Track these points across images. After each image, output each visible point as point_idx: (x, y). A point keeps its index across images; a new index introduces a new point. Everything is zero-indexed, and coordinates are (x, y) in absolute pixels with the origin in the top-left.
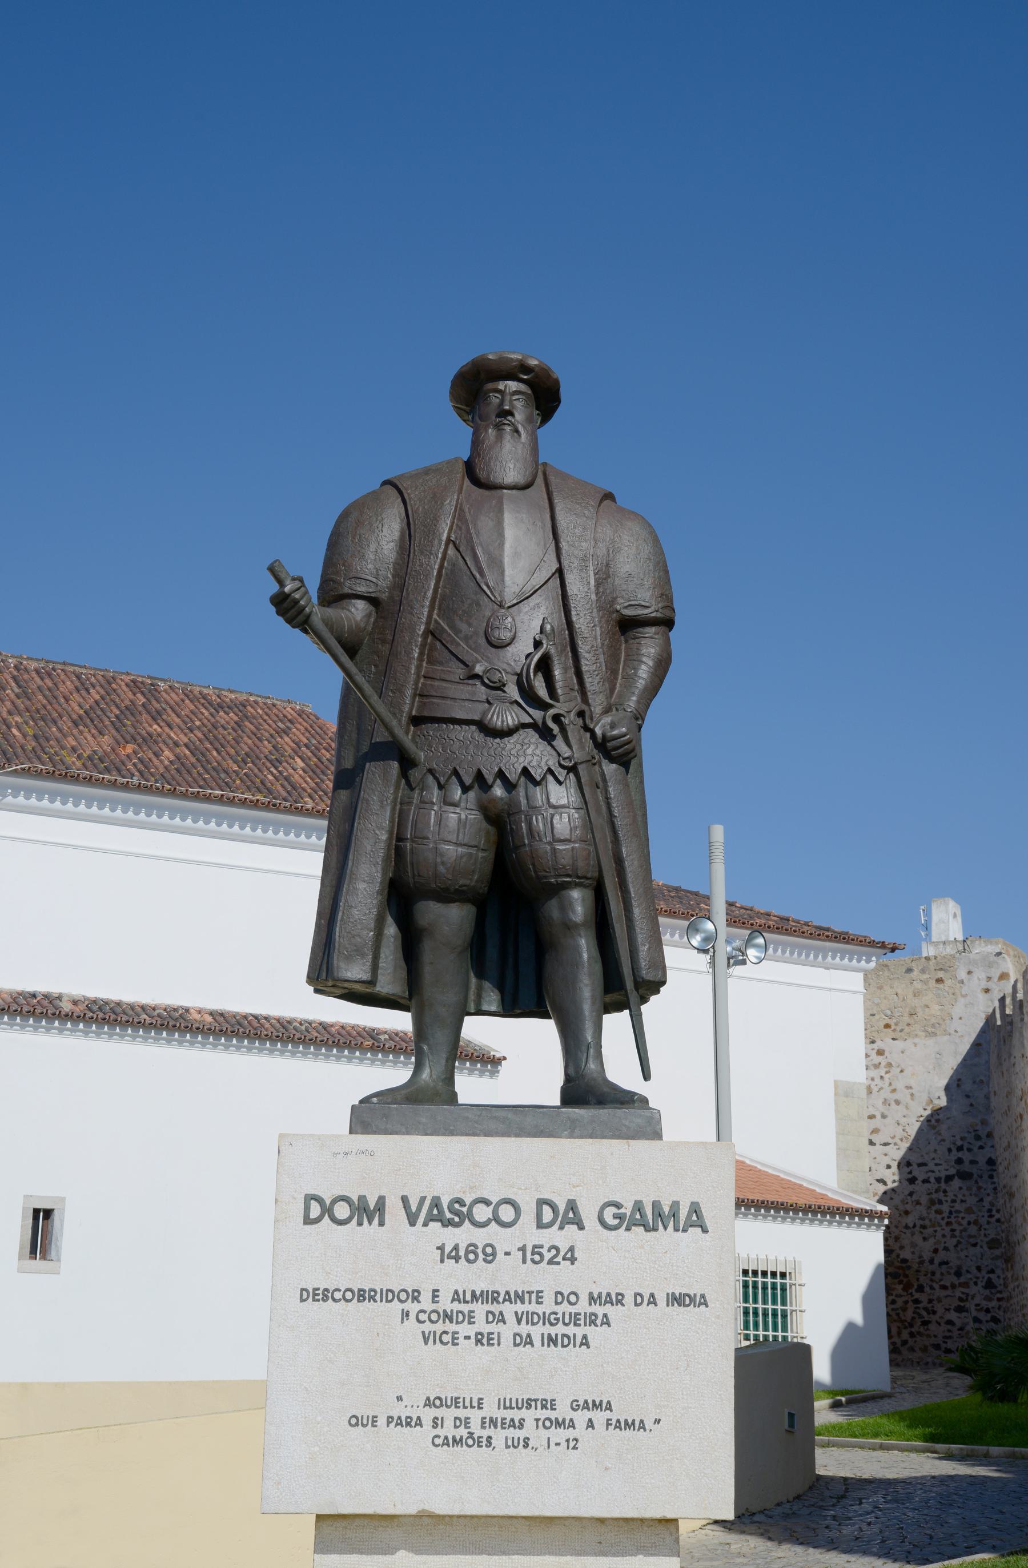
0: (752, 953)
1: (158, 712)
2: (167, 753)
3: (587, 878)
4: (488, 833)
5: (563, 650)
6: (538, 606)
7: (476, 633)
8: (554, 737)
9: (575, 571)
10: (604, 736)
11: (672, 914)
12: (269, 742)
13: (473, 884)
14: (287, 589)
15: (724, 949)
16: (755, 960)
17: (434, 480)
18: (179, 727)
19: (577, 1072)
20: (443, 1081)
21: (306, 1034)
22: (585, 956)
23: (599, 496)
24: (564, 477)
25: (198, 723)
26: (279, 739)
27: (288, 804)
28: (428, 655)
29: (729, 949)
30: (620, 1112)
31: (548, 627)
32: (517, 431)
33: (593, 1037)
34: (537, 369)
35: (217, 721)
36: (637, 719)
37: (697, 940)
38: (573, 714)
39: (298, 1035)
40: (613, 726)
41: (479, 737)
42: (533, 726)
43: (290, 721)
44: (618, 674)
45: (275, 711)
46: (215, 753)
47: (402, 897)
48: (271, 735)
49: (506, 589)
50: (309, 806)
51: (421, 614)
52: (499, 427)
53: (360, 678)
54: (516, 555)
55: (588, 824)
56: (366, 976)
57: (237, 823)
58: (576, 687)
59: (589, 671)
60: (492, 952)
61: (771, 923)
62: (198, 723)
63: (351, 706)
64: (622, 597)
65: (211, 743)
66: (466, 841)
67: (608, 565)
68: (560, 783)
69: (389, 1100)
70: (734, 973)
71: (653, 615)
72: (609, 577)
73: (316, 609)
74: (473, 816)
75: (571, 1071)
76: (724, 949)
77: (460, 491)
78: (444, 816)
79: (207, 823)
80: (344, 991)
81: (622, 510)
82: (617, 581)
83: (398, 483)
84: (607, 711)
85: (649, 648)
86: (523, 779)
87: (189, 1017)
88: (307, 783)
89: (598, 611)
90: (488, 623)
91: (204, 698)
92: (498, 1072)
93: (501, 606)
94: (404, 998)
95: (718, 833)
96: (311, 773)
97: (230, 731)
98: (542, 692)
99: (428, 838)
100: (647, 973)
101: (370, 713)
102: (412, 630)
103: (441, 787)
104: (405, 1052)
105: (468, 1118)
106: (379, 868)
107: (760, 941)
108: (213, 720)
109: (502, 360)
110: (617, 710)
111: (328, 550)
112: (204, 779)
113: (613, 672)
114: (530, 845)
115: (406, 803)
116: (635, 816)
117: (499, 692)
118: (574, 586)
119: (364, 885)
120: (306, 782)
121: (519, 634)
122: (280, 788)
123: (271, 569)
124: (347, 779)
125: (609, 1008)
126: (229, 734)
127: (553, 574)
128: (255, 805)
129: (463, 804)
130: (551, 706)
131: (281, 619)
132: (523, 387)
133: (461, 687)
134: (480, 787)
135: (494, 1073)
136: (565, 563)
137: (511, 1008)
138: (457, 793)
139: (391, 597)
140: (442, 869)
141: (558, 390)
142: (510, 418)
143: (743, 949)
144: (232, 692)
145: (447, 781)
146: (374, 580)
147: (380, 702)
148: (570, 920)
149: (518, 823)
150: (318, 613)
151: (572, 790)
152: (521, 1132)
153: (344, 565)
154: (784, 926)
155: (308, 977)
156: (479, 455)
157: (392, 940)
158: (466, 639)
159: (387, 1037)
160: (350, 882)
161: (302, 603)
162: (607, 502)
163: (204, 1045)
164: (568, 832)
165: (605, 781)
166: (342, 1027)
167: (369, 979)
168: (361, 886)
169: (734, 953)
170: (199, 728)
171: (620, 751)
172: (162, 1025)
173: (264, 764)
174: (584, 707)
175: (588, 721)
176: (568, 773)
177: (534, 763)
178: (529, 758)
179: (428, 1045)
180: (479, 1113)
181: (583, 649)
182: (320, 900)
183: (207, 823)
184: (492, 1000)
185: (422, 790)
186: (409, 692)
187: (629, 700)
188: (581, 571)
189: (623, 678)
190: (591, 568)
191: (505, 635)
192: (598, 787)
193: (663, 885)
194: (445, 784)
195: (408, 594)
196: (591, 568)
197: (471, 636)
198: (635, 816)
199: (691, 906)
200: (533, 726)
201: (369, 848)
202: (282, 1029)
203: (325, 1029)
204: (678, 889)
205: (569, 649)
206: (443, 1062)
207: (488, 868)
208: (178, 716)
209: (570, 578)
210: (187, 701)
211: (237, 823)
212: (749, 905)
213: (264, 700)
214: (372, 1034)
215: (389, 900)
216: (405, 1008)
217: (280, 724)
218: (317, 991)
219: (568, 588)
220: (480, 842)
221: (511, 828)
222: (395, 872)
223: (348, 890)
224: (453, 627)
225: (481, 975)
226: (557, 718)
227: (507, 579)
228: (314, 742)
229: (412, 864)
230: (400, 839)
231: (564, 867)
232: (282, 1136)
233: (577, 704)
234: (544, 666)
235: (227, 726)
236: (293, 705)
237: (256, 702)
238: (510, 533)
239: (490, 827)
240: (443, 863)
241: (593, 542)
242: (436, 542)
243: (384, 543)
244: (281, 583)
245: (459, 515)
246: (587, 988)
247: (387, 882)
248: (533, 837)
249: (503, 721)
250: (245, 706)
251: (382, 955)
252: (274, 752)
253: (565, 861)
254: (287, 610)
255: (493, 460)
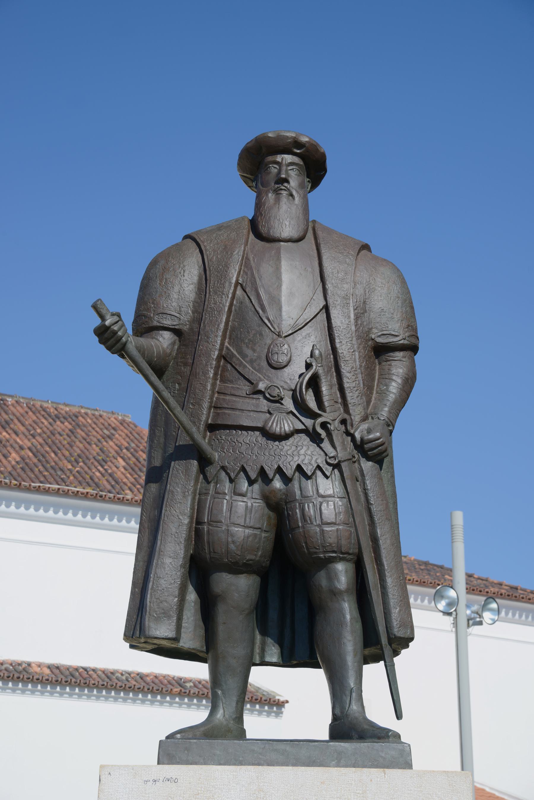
0: (487, 616)
1: (7, 422)
2: (14, 455)
3: (349, 554)
4: (269, 517)
5: (329, 371)
6: (309, 335)
7: (259, 357)
8: (322, 440)
9: (338, 307)
10: (362, 439)
11: (422, 584)
12: (97, 446)
13: (257, 559)
14: (107, 323)
15: (465, 612)
16: (491, 622)
17: (225, 235)
18: (24, 434)
19: (342, 712)
20: (234, 720)
21: (127, 683)
22: (348, 617)
23: (358, 247)
24: (329, 231)
25: (39, 431)
26: (105, 443)
27: (112, 495)
28: (221, 375)
29: (468, 612)
30: (377, 745)
31: (317, 352)
32: (291, 195)
33: (355, 683)
34: (307, 145)
35: (55, 429)
36: (388, 426)
37: (442, 605)
38: (337, 422)
39: (119, 684)
40: (369, 431)
41: (262, 440)
42: (305, 431)
43: (114, 429)
44: (373, 389)
45: (102, 420)
46: (53, 455)
47: (201, 569)
48: (99, 440)
49: (283, 322)
50: (129, 497)
51: (215, 342)
52: (277, 192)
53: (166, 394)
54: (291, 294)
55: (350, 510)
56: (171, 634)
57: (71, 511)
58: (340, 400)
59: (350, 387)
60: (273, 615)
61: (503, 591)
62: (39, 431)
63: (159, 415)
64: (376, 328)
65: (50, 447)
66: (252, 524)
67: (364, 302)
68: (327, 477)
69: (190, 736)
70: (473, 632)
71: (401, 342)
72: (366, 311)
73: (131, 339)
74: (258, 504)
75: (338, 712)
76: (465, 612)
77: (246, 244)
78: (234, 504)
79: (46, 511)
80: (154, 647)
81: (376, 258)
82: (372, 315)
83: (196, 237)
84: (365, 419)
85: (398, 367)
86: (297, 474)
87: (31, 670)
88: (128, 479)
89: (357, 339)
90: (269, 349)
91: (44, 410)
92: (282, 713)
93: (279, 336)
94: (202, 652)
95: (459, 517)
96: (131, 471)
97: (66, 437)
98: (312, 404)
99: (221, 522)
100: (398, 631)
101: (175, 422)
102: (208, 355)
103: (231, 481)
104: (200, 696)
105: (253, 751)
106: (182, 546)
107: (494, 606)
108: (51, 428)
109: (279, 137)
110: (372, 418)
111: (140, 291)
112: (44, 476)
113: (370, 388)
114: (303, 527)
115: (203, 493)
116: (387, 504)
117: (278, 405)
118: (338, 319)
119: (170, 560)
120: (126, 477)
121: (293, 358)
122: (105, 483)
123: (95, 307)
124: (156, 475)
125: (368, 660)
126: (64, 439)
127: (321, 310)
128: (86, 496)
129: (249, 495)
130: (320, 416)
131: (102, 347)
132: (296, 159)
133: (247, 400)
134: (263, 481)
135: (278, 714)
136: (330, 301)
137: (289, 660)
138: (244, 485)
139: (191, 329)
140: (232, 547)
141: (325, 162)
142: (286, 184)
143: (480, 612)
144: (66, 405)
145: (237, 476)
146: (178, 315)
147: (183, 412)
148: (336, 588)
149: (293, 509)
150: (132, 342)
151: (337, 483)
152: (297, 762)
153: (153, 303)
154: (513, 594)
155: (125, 635)
156: (261, 215)
157: (193, 604)
158: (251, 362)
159: (192, 684)
160: (159, 558)
161: (120, 333)
162: (364, 252)
163: (42, 693)
164: (334, 516)
165: (363, 475)
166: (156, 677)
167: (174, 636)
168: (168, 561)
169: (473, 615)
170: (40, 435)
171: (375, 451)
172: (8, 677)
173: (92, 463)
174: (346, 416)
175: (349, 428)
176: (333, 469)
177: (306, 461)
178: (302, 457)
179: (222, 690)
180: (263, 746)
181: (345, 369)
182: (134, 572)
183: (46, 511)
184: (273, 653)
185: (216, 483)
186: (206, 405)
187: (382, 410)
188: (343, 307)
189: (377, 393)
190: (351, 305)
191: (283, 359)
192: (358, 481)
193: (415, 560)
194: (235, 478)
195: (205, 326)
196: (351, 305)
197: (256, 360)
198: (387, 504)
199: (436, 577)
200: (305, 431)
201: (174, 530)
202: (106, 679)
203: (141, 678)
204: (426, 563)
205: (333, 370)
206: (234, 704)
207: (270, 546)
208: (23, 425)
209: (335, 313)
210: (30, 413)
211: (71, 511)
212: (484, 576)
213: (93, 412)
214: (180, 682)
215: (190, 573)
216: (204, 661)
217: (106, 431)
218: (132, 647)
219: (333, 321)
220: (263, 525)
221: (288, 514)
222: (195, 550)
223: (157, 564)
224: (241, 353)
225: (264, 633)
226: (324, 425)
227: (284, 314)
228: (133, 445)
229: (209, 543)
230: (199, 522)
231: (331, 544)
232: (102, 767)
233: (340, 414)
234: (314, 383)
235: (62, 433)
236: (116, 416)
237: (86, 414)
238: (286, 277)
239: (271, 513)
240: (233, 542)
241: (353, 284)
242: (227, 284)
243: (186, 285)
244: (102, 317)
245: (246, 262)
246: (350, 643)
247: (189, 557)
248: (305, 520)
249: (281, 428)
250: (77, 417)
251: (185, 617)
252: (101, 453)
253: (331, 540)
254: (108, 340)
255: (272, 219)
